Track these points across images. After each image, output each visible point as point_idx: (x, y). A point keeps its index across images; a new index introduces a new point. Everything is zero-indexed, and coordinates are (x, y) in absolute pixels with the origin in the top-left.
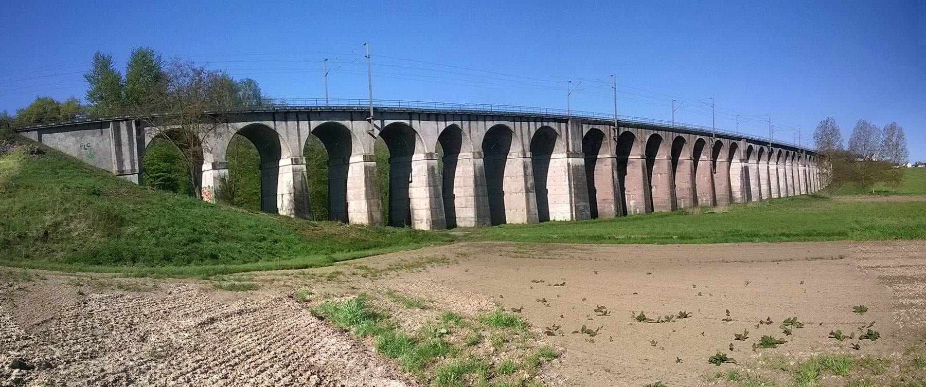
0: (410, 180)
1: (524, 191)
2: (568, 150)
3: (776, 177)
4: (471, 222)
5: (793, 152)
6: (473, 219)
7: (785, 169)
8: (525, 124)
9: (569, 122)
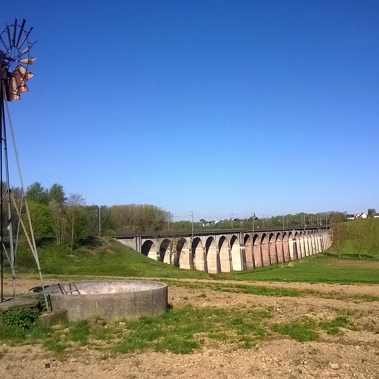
0: (194, 256)
1: (229, 260)
2: (240, 244)
3: (307, 245)
4: (215, 272)
5: (314, 230)
6: (216, 271)
7: (311, 240)
8: (229, 235)
9: (241, 233)
